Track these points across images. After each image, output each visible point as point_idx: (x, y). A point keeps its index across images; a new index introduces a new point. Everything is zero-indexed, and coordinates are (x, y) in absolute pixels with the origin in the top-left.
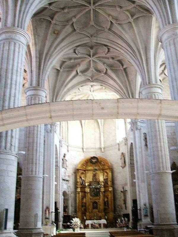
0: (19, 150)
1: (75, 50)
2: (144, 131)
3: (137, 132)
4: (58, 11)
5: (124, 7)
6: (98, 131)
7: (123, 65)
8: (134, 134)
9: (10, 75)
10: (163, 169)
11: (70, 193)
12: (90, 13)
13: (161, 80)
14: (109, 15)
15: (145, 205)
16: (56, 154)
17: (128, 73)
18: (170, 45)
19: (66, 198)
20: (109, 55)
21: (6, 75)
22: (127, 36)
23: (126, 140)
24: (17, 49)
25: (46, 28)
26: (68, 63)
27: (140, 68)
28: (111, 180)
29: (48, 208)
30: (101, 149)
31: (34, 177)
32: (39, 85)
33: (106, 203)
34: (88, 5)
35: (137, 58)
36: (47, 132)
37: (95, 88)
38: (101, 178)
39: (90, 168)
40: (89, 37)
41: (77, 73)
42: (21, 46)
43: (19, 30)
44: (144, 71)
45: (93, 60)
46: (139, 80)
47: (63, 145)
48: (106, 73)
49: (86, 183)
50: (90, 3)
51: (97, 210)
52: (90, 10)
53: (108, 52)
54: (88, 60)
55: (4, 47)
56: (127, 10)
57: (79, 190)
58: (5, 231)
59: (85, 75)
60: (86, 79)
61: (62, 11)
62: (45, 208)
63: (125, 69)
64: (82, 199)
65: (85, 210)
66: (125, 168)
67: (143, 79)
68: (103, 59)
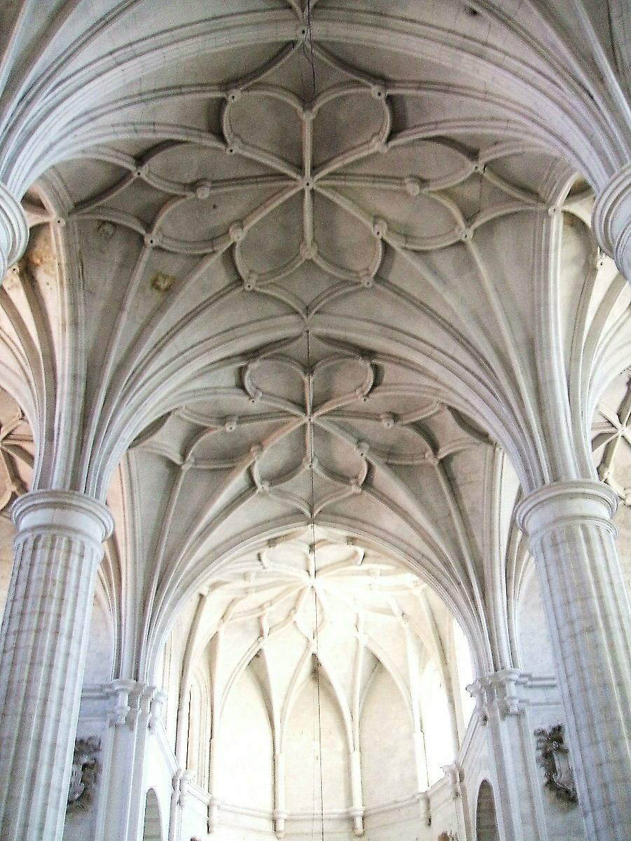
1: (241, 371)
2: (542, 720)
3: (507, 729)
4: (178, 193)
5: (433, 181)
6: (340, 746)
7: (435, 449)
8: (496, 734)
12: (302, 201)
14: (377, 218)
20: (378, 401)
25: (122, 266)
26: (215, 437)
30: (351, 819)
32: (75, 486)
34: (294, 175)
35: (498, 386)
37: (326, 555)
40: (297, 313)
41: (252, 485)
44: (532, 437)
45: (313, 425)
46: (509, 479)
47: (187, 800)
48: (368, 483)
50: (300, 168)
52: (303, 192)
53: (374, 386)
54: (295, 425)
56: (445, 192)
59: (282, 494)
60: (285, 510)
61: (190, 195)
63: (445, 463)
68: (357, 423)
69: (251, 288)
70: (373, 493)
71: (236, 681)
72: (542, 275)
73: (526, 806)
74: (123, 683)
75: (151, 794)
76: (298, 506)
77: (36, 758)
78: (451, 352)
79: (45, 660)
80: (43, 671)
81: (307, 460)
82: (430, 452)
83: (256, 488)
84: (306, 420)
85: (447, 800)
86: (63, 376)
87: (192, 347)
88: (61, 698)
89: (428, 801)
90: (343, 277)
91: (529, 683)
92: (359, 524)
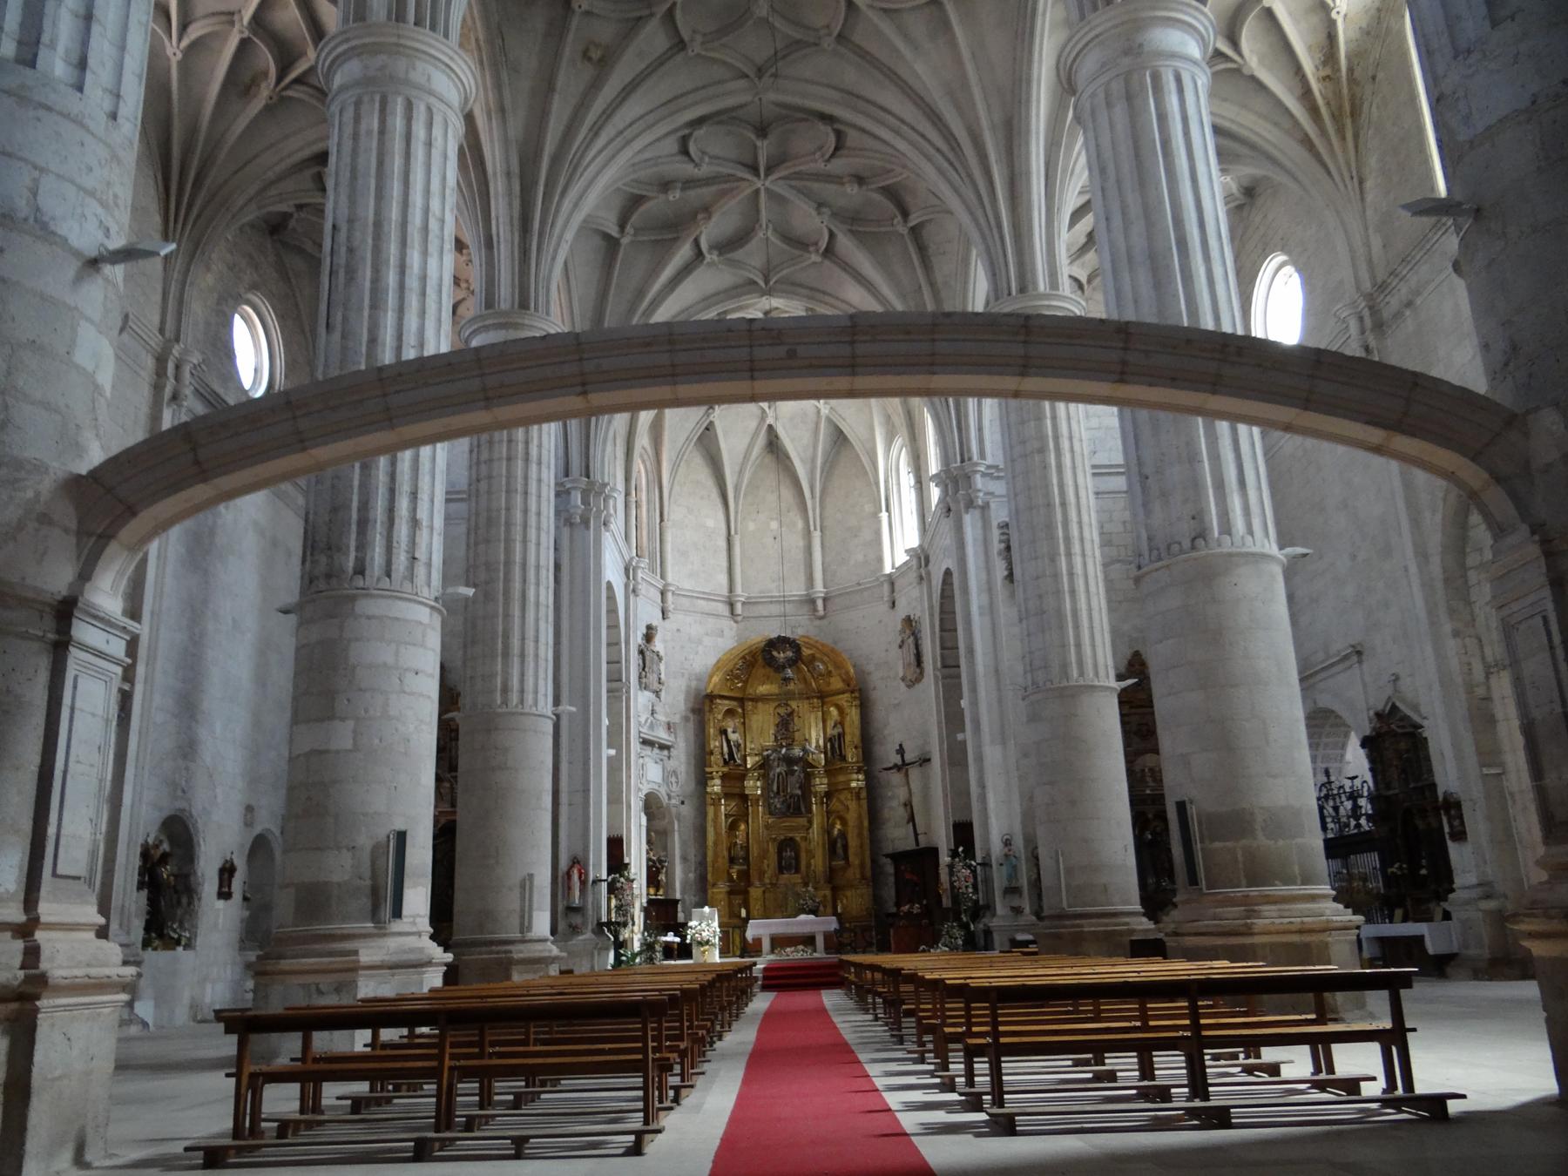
0: (447, 579)
1: (684, 142)
3: (970, 521)
6: (800, 524)
7: (905, 214)
8: (959, 528)
9: (393, 249)
10: (1082, 674)
11: (673, 801)
13: (1084, 280)
15: (1007, 843)
16: (613, 627)
17: (932, 249)
18: (1109, 105)
19: (660, 824)
20: (839, 165)
21: (377, 250)
22: (924, 71)
23: (921, 557)
24: (419, 131)
26: (656, 205)
27: (982, 221)
28: (857, 740)
29: (578, 862)
30: (812, 602)
31: (513, 714)
32: (524, 305)
33: (835, 846)
35: (970, 176)
36: (569, 523)
38: (814, 736)
39: (763, 689)
40: (747, 76)
41: (699, 254)
42: (438, 119)
43: (425, 40)
45: (767, 190)
47: (642, 588)
48: (829, 252)
49: (748, 758)
51: (797, 878)
53: (837, 149)
55: (357, 119)
57: (717, 789)
58: (396, 926)
62: (564, 864)
63: (915, 231)
64: (733, 827)
65: (745, 876)
66: (919, 687)
67: (994, 275)
68: (816, 186)
69: (695, 52)
70: (835, 262)
71: (685, 457)
72: (1026, 43)
73: (985, 598)
74: (573, 481)
75: (610, 586)
76: (751, 276)
77: (524, 581)
78: (921, 129)
79: (520, 488)
80: (519, 499)
81: (761, 226)
82: (899, 218)
83: (704, 258)
84: (759, 184)
85: (911, 584)
86: (495, 174)
87: (630, 125)
88: (539, 522)
89: (892, 584)
90: (798, 36)
91: (996, 474)
92: (820, 296)
